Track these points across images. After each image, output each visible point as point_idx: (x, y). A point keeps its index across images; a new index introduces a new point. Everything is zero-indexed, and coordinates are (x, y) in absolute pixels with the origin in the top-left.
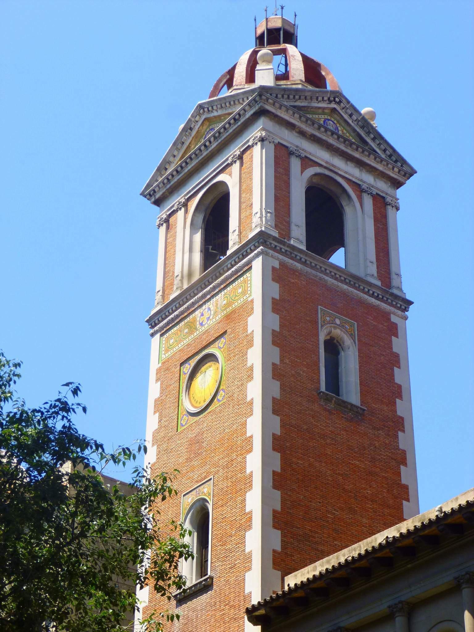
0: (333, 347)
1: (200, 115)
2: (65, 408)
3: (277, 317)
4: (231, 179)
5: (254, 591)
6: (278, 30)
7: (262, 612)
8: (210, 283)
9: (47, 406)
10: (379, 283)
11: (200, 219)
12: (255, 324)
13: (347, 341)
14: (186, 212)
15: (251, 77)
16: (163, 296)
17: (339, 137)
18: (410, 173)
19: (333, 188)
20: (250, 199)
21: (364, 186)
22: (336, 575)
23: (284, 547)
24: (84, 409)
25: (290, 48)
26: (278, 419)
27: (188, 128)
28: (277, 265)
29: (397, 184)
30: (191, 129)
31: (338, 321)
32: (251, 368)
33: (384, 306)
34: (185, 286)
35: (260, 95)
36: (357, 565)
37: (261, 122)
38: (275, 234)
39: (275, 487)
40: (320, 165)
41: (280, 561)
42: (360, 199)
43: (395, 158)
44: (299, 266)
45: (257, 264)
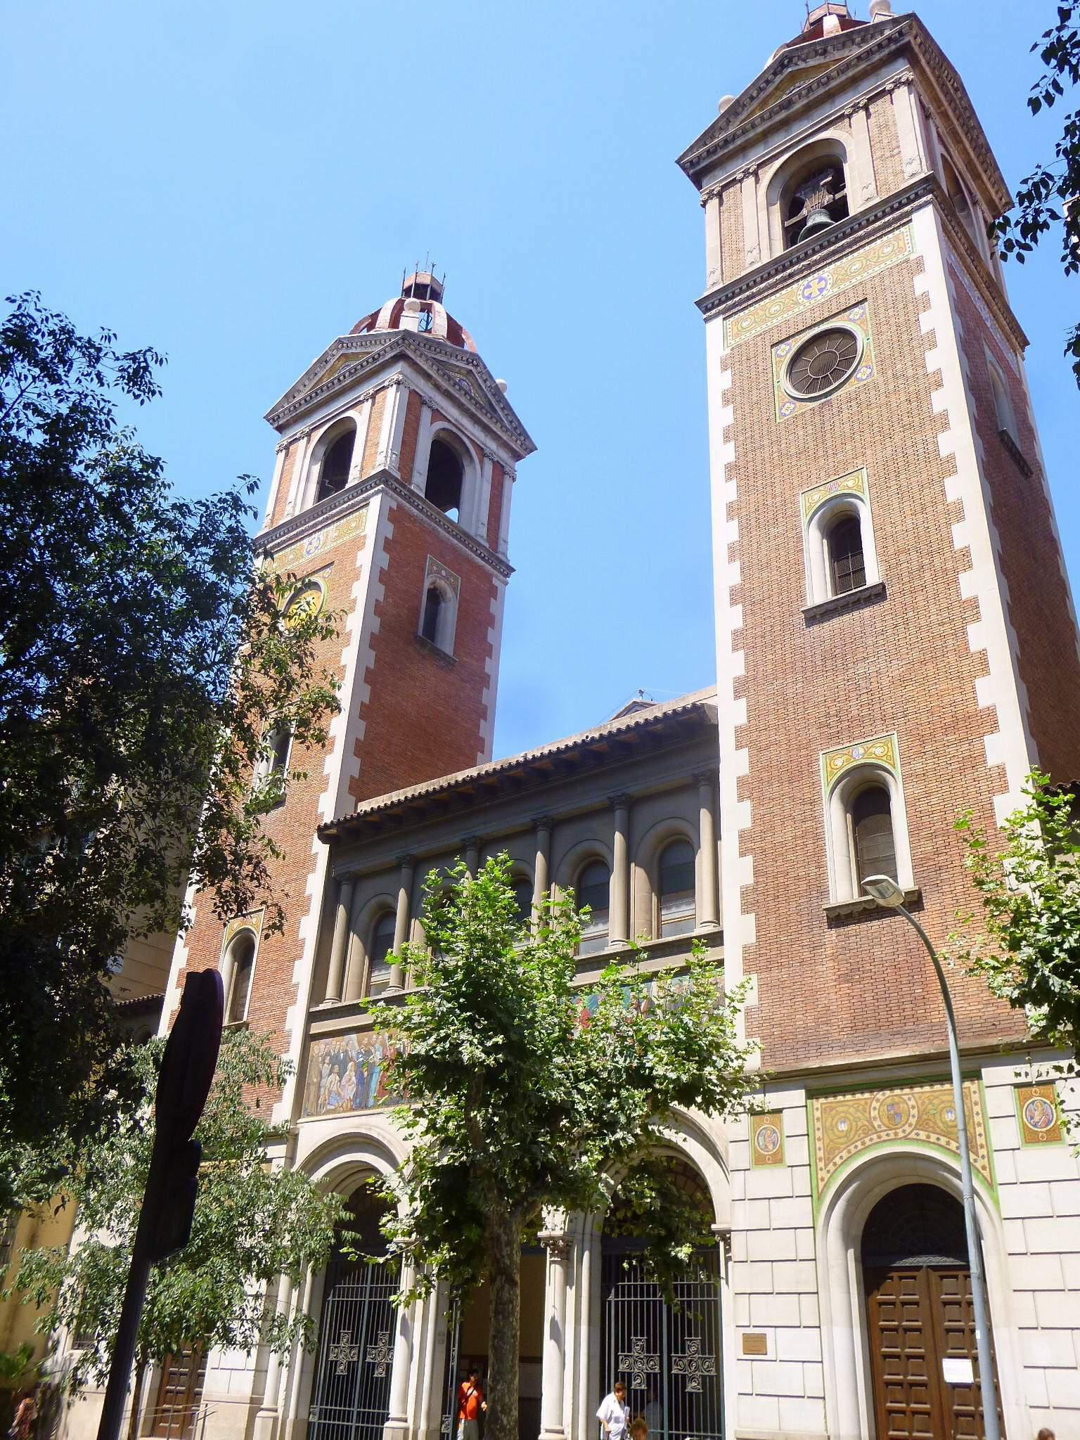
0: (435, 596)
1: (338, 349)
2: (236, 504)
3: (388, 556)
4: (360, 417)
5: (327, 809)
6: (425, 286)
7: (333, 831)
8: (323, 514)
9: (216, 499)
10: (487, 545)
11: (321, 452)
12: (365, 559)
13: (450, 593)
14: (308, 441)
15: (395, 322)
16: (272, 521)
17: (471, 398)
18: (532, 448)
19: (457, 446)
20: (378, 437)
21: (487, 451)
22: (415, 804)
23: (362, 771)
24: (255, 515)
25: (436, 304)
26: (373, 653)
27: (323, 360)
28: (395, 507)
29: (518, 457)
30: (326, 362)
31: (443, 573)
32: (355, 601)
33: (488, 567)
34: (297, 513)
35: (403, 339)
36: (437, 797)
37: (400, 366)
38: (398, 475)
39: (361, 717)
40: (449, 421)
41: (356, 787)
42: (481, 462)
43: (519, 430)
44: (415, 511)
45: (376, 502)
